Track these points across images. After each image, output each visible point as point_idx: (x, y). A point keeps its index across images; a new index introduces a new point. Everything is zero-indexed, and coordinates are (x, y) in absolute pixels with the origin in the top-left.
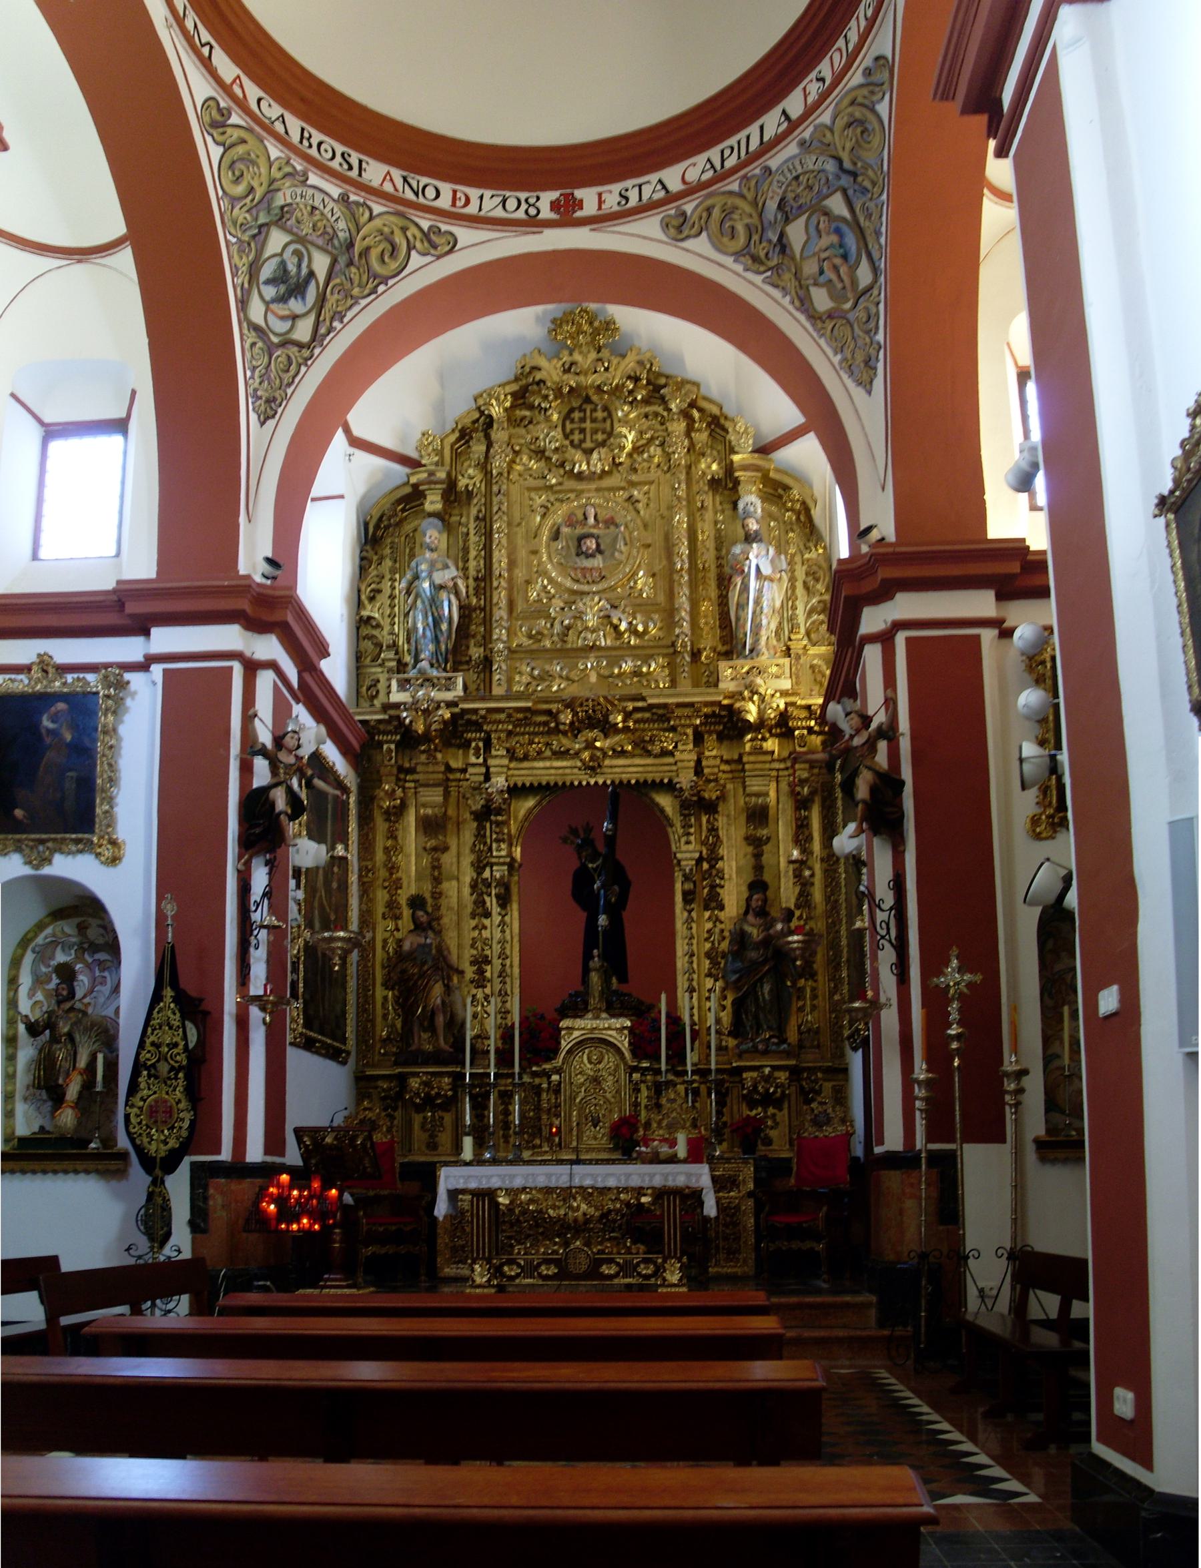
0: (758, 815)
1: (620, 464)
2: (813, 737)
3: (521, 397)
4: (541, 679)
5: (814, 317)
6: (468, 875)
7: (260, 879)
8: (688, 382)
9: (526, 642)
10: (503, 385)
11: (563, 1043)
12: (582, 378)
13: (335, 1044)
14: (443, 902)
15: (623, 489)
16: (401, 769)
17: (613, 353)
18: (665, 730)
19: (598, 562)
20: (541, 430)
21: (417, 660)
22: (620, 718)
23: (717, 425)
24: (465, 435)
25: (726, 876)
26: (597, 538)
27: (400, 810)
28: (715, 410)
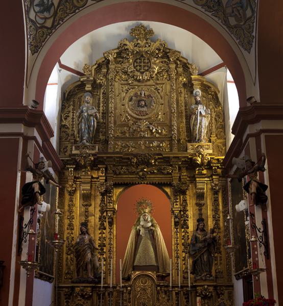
0: (200, 196)
1: (153, 77)
2: (219, 170)
3: (119, 54)
4: (125, 147)
5: (229, 27)
6: (98, 215)
7: (27, 216)
8: (177, 51)
9: (120, 135)
10: (114, 50)
11: (133, 276)
12: (141, 49)
13: (50, 275)
14: (89, 224)
15: (153, 85)
16: (75, 177)
17: (152, 41)
18: (168, 166)
19: (145, 109)
20: (125, 65)
21: (82, 139)
22: (153, 161)
23: (186, 66)
24: (99, 67)
25: (189, 217)
26: (145, 101)
27: (75, 191)
28: (185, 61)
